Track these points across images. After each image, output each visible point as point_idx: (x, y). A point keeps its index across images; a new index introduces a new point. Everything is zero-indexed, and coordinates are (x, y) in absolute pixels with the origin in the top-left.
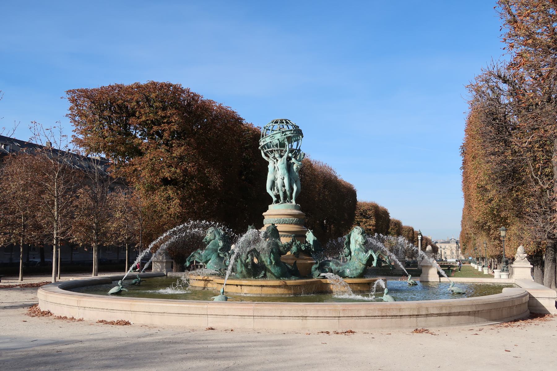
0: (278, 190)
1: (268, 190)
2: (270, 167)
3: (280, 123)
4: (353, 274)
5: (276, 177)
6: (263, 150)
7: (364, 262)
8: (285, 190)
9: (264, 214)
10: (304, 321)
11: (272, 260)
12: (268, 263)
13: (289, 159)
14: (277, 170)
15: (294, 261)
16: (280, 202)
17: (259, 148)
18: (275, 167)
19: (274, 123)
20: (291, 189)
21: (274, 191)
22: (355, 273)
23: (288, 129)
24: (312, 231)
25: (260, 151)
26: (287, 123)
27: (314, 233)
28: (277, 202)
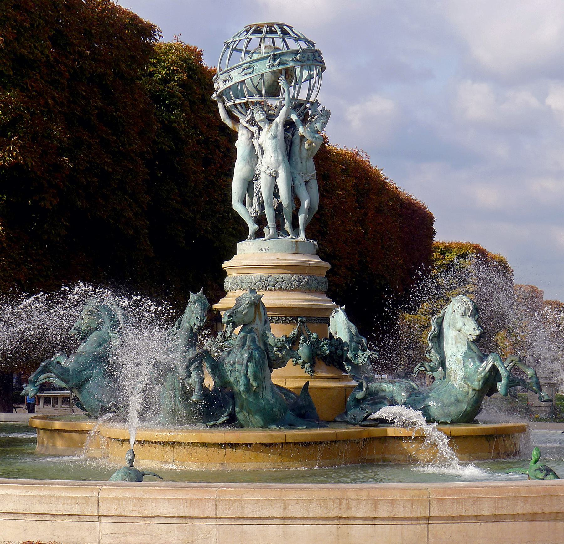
0: (262, 205)
1: (237, 206)
2: (241, 145)
3: (267, 32)
4: (449, 415)
5: (257, 172)
6: (224, 102)
7: (477, 385)
8: (280, 204)
9: (225, 264)
10: (343, 528)
11: (251, 381)
12: (242, 388)
13: (289, 125)
14: (260, 154)
15: (302, 384)
16: (266, 237)
17: (214, 96)
18: (253, 145)
19: (252, 34)
20: (296, 200)
21: (251, 205)
22: (454, 411)
23: (286, 50)
24: (343, 307)
25: (215, 103)
26: (285, 33)
27: (351, 315)
28: (259, 234)
